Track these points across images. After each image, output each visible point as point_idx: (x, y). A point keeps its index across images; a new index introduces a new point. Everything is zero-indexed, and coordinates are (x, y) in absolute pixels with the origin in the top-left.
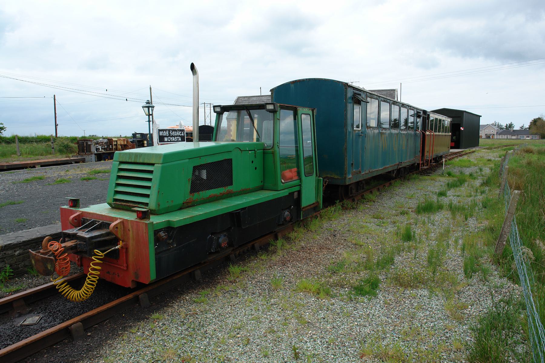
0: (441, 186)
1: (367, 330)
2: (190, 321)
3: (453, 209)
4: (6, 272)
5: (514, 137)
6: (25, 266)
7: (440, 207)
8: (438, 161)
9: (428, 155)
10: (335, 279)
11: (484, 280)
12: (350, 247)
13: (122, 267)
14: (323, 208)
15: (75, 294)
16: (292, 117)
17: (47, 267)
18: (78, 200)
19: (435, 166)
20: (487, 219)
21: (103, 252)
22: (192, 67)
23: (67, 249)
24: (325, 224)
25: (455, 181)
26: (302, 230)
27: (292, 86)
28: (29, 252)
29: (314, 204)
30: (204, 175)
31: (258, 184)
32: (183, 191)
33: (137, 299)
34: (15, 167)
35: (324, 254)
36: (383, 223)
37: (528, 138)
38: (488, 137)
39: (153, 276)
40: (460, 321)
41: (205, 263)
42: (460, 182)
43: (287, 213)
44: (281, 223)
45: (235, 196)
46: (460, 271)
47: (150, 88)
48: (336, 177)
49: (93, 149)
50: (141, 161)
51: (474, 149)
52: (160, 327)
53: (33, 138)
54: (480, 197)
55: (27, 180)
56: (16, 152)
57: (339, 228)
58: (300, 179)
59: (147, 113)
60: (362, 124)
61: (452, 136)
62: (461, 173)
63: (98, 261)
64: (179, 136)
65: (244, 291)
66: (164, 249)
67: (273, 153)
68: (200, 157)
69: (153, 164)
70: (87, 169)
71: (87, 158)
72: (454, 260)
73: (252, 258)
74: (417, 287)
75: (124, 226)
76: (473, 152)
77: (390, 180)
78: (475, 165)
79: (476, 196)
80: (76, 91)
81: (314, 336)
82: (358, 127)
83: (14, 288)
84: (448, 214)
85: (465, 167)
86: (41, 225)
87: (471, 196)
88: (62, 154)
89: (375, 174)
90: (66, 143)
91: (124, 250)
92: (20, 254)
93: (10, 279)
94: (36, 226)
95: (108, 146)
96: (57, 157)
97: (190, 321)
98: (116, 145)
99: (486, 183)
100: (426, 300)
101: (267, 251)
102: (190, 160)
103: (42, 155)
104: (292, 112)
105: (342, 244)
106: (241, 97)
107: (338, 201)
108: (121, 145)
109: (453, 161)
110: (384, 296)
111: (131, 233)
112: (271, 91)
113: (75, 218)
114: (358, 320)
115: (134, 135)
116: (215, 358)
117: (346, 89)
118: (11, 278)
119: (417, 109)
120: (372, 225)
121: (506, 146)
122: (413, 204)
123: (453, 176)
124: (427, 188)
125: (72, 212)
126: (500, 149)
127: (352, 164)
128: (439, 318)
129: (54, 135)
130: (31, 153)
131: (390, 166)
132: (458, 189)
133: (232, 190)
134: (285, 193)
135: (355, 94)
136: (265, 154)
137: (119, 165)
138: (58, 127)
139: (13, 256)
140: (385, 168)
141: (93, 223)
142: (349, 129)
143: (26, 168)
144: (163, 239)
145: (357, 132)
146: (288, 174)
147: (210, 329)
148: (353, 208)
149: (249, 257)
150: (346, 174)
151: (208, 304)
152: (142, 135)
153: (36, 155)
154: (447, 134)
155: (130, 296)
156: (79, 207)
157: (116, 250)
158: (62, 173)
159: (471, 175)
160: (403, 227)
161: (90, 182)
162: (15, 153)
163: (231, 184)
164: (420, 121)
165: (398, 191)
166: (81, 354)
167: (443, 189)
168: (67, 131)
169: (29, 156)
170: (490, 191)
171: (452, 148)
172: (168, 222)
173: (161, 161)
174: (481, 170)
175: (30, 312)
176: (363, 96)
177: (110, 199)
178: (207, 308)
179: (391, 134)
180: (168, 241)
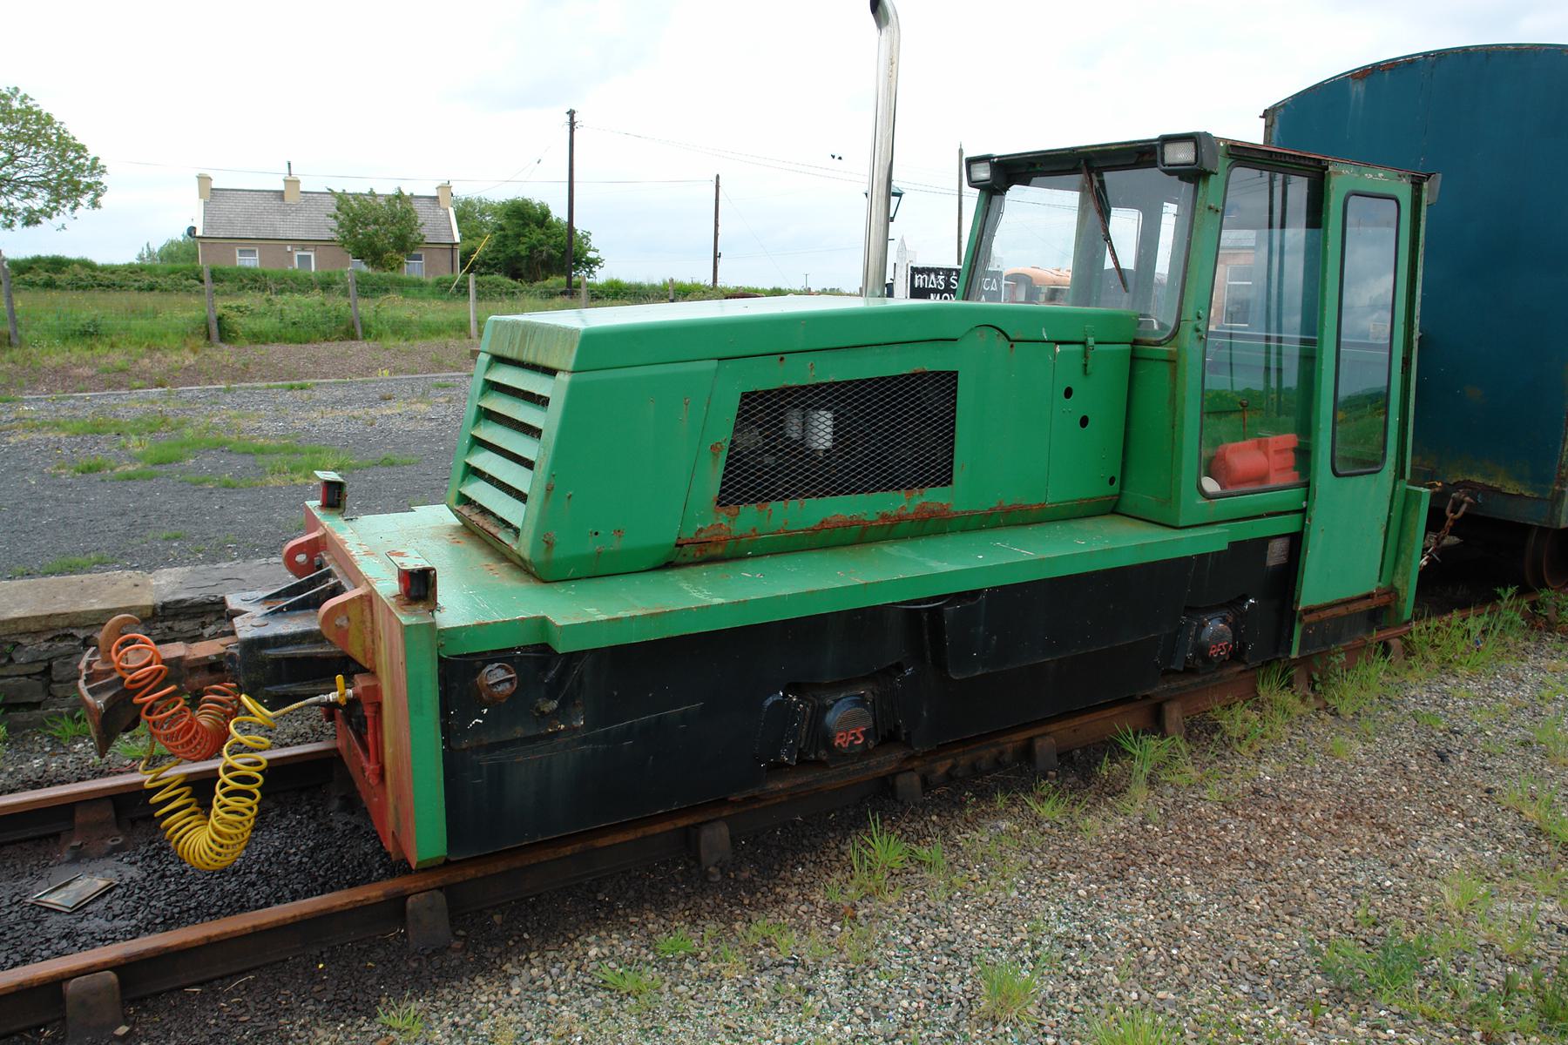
12: (1500, 839)
14: (1417, 617)
24: (1418, 690)
27: (1358, 88)
29: (1369, 596)
31: (1097, 488)
32: (688, 490)
33: (395, 907)
44: (1178, 666)
45: (964, 530)
48: (1511, 488)
53: (653, 287)
57: (1480, 719)
58: (1307, 485)
66: (519, 732)
67: (1172, 362)
68: (781, 355)
69: (551, 372)
73: (1001, 801)
102: (728, 364)
105: (1463, 815)
107: (1510, 591)
112: (1265, 115)
129: (710, 282)
133: (944, 508)
134: (1215, 540)
138: (721, 262)
146: (1244, 457)
149: (985, 795)
163: (944, 477)
172: (543, 622)
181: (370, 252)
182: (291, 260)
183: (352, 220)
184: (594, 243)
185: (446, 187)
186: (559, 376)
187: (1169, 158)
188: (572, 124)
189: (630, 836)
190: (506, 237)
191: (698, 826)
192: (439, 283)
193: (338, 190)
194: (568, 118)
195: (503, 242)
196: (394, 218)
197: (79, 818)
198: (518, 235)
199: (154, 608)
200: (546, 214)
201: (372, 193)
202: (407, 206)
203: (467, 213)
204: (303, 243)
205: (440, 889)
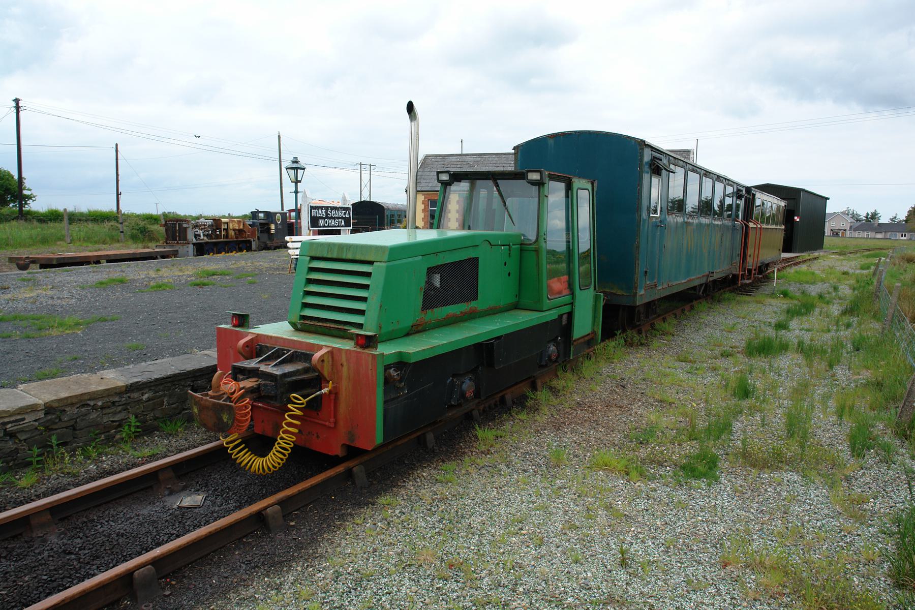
0: (775, 313)
1: (721, 529)
2: (441, 509)
3: (801, 348)
4: (130, 426)
5: (879, 236)
6: (156, 418)
7: (784, 347)
8: (763, 268)
9: (751, 263)
10: (643, 453)
11: (887, 460)
13: (327, 423)
15: (258, 463)
16: (562, 194)
17: (221, 419)
18: (248, 315)
19: (759, 280)
20: (868, 368)
21: (305, 397)
22: (410, 107)
23: (250, 391)
25: (796, 305)
26: (569, 375)
27: (551, 142)
28: (187, 393)
30: (437, 281)
31: (511, 299)
32: (411, 309)
33: (349, 474)
34: (70, 261)
35: (616, 415)
36: (697, 369)
37: (903, 238)
38: (835, 234)
39: (379, 439)
40: (860, 519)
41: (440, 421)
42: (805, 308)
43: (552, 348)
45: (480, 317)
46: (844, 448)
47: (279, 137)
48: (619, 293)
49: (190, 236)
50: (350, 257)
51: (816, 254)
52: (398, 517)
53: (82, 214)
54: (844, 333)
55: (101, 283)
56: (63, 236)
58: (573, 294)
59: (293, 179)
60: (661, 208)
61: (785, 230)
62: (803, 293)
63: (299, 413)
64: (342, 218)
65: (508, 466)
67: (537, 251)
69: (371, 263)
70: (190, 268)
71: (181, 249)
72: (829, 430)
74: (778, 469)
75: (333, 358)
76: (815, 259)
77: (691, 301)
78: (823, 281)
79: (837, 331)
80: (159, 139)
81: (641, 536)
82: (655, 211)
83: (147, 452)
84: (799, 359)
85: (807, 282)
86: (173, 355)
87: (829, 331)
88: (136, 243)
89: (675, 291)
90: (142, 224)
91: (332, 397)
92: (149, 399)
93: (136, 437)
94: (163, 357)
96: (128, 248)
97: (441, 509)
98: (226, 230)
99: (850, 311)
100: (801, 490)
101: (524, 407)
103: (104, 243)
104: (562, 185)
105: (639, 401)
106: (430, 156)
108: (234, 230)
109: (784, 272)
110: (729, 481)
111: (345, 369)
112: (514, 148)
113: (247, 345)
114: (702, 514)
115: (254, 214)
116: (498, 564)
117: (642, 149)
118: (138, 436)
119: (738, 184)
120: (680, 373)
121: (869, 250)
122: (738, 340)
123: (791, 298)
124: (756, 314)
125: (240, 336)
126: (858, 255)
127: (646, 272)
128: (827, 515)
129: (115, 209)
130: (88, 239)
131: (696, 278)
132: (804, 318)
135: (654, 158)
136: (525, 252)
137: (310, 262)
138: (122, 197)
139: (140, 401)
140: (690, 280)
142: (644, 215)
143: (88, 263)
144: (395, 380)
145: (654, 220)
147: (476, 521)
148: (642, 344)
150: (636, 289)
151: (459, 485)
152: (267, 214)
153: (96, 242)
154: (778, 227)
155: (340, 469)
156: (249, 328)
157: (321, 395)
158: (152, 274)
159: (821, 296)
160: (733, 377)
161: (206, 288)
162: (61, 239)
163: (476, 298)
164: (741, 203)
165: (707, 318)
166: (289, 552)
167: (783, 317)
168: (136, 204)
169: (85, 245)
170: (860, 324)
171: (784, 251)
173: (386, 258)
174: (835, 289)
175: (184, 489)
176: (665, 161)
177: (295, 315)
178: (461, 490)
179: (701, 224)
180: (397, 384)
187: (530, 177)
188: (18, 108)
189: (406, 440)
191: (424, 434)
194: (14, 104)
197: (161, 477)
199: (127, 386)
205: (361, 464)
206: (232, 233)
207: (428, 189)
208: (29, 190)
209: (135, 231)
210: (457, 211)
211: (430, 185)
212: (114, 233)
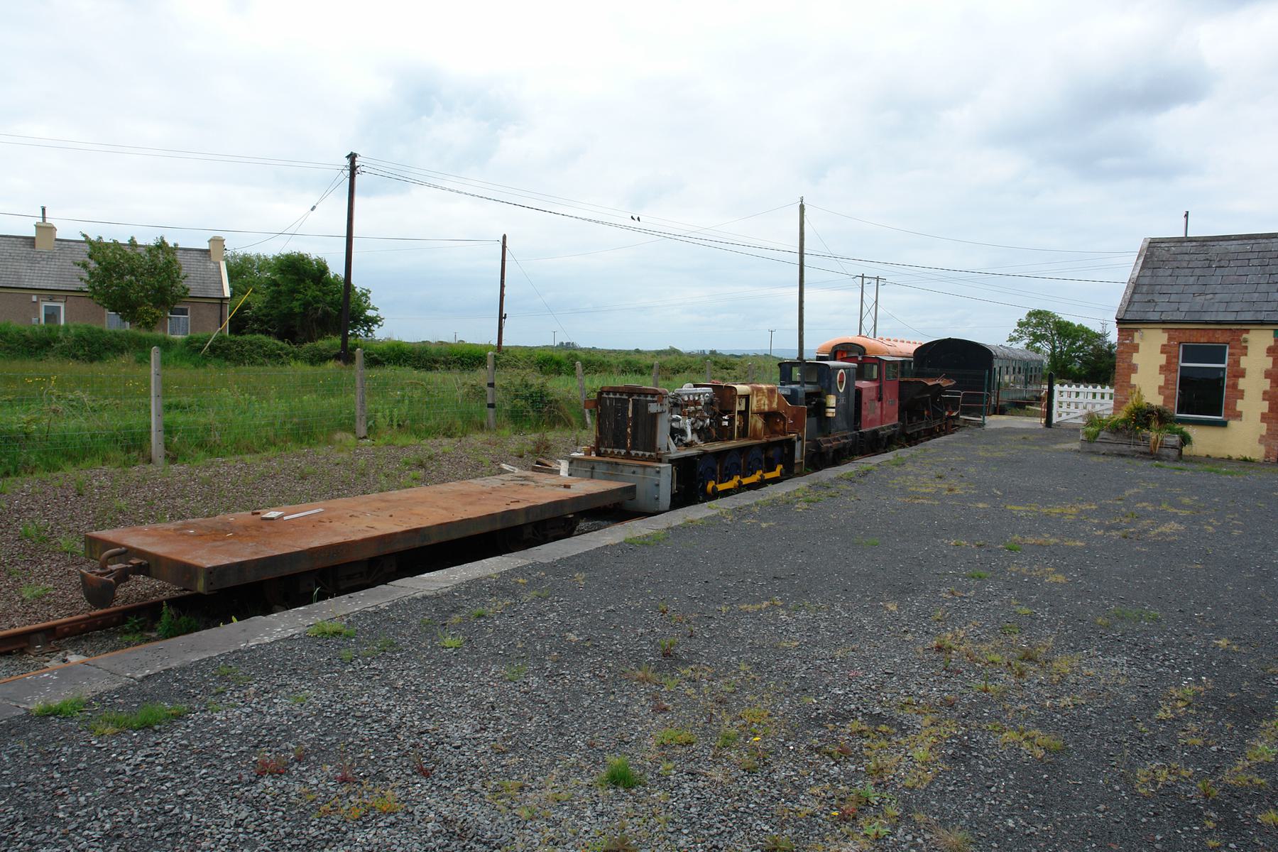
47: (802, 208)
95: (717, 418)
129: (495, 342)
138: (506, 322)
141: (405, 361)
181: (124, 305)
182: (37, 312)
183: (106, 269)
184: (373, 302)
185: (217, 242)
186: (878, 404)
188: (353, 170)
190: (280, 292)
192: (189, 342)
193: (94, 238)
194: (347, 162)
195: (276, 298)
196: (153, 270)
198: (293, 291)
200: (322, 269)
201: (133, 243)
202: (170, 257)
203: (241, 270)
204: (52, 294)
206: (757, 423)
207: (1180, 317)
208: (374, 309)
209: (520, 403)
210: (1133, 369)
211: (1184, 307)
212: (474, 406)
